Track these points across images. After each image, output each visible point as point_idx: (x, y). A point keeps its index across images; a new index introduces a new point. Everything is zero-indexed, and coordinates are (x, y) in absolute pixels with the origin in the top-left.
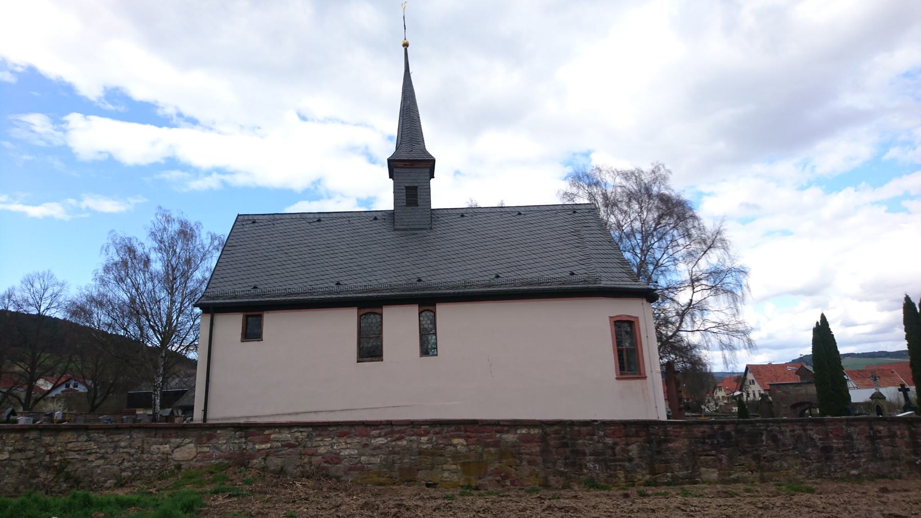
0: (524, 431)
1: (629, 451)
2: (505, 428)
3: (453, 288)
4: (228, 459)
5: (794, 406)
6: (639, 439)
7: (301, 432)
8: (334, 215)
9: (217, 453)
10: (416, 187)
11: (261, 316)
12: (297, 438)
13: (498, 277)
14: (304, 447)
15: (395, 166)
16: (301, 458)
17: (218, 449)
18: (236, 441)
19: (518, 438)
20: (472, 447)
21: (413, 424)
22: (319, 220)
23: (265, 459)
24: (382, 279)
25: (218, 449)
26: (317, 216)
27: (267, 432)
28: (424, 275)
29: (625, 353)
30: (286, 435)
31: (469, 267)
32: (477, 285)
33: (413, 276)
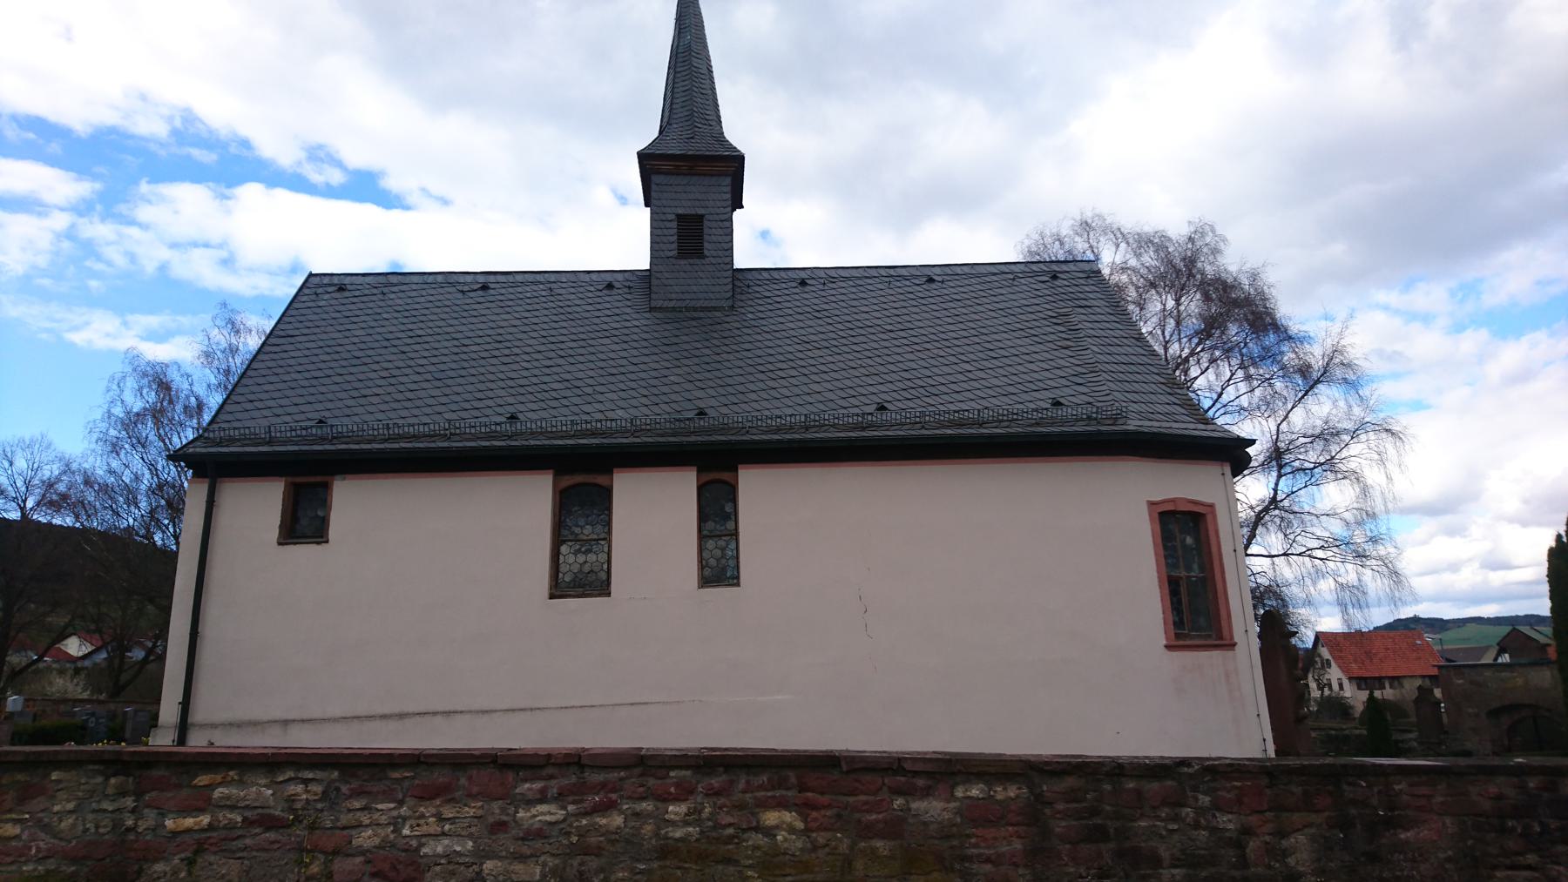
0: (975, 792)
1: (1285, 853)
2: (921, 782)
3: (778, 430)
4: (74, 860)
5: (1495, 713)
6: (1313, 817)
7: (306, 782)
8: (519, 278)
9: (44, 842)
10: (702, 216)
11: (326, 487)
12: (291, 800)
13: (882, 408)
14: (312, 827)
15: (655, 166)
16: (300, 863)
17: (46, 828)
18: (106, 805)
19: (958, 812)
20: (821, 838)
21: (643, 764)
22: (485, 287)
23: (191, 862)
24: (619, 409)
25: (46, 828)
26: (481, 279)
27: (202, 780)
28: (713, 402)
29: (1183, 589)
30: (260, 791)
31: (816, 387)
32: (834, 426)
33: (688, 405)
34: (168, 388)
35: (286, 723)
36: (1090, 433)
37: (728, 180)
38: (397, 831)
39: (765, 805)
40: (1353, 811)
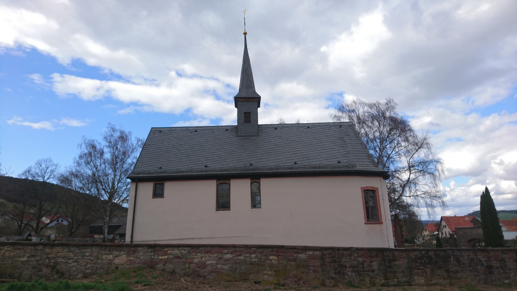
1: (372, 266)
2: (300, 251)
3: (270, 169)
4: (144, 264)
5: (469, 241)
7: (185, 250)
8: (204, 128)
9: (138, 261)
11: (163, 184)
12: (182, 253)
13: (296, 163)
14: (186, 258)
16: (184, 265)
17: (138, 258)
18: (149, 254)
20: (281, 261)
21: (247, 247)
22: (196, 131)
23: (164, 265)
25: (138, 258)
26: (195, 129)
27: (166, 249)
30: (176, 252)
31: (279, 157)
32: (284, 168)
33: (248, 162)
34: (95, 148)
35: (182, 239)
36: (346, 171)
37: (257, 103)
38: (202, 259)
39: (270, 255)
40: (386, 258)
